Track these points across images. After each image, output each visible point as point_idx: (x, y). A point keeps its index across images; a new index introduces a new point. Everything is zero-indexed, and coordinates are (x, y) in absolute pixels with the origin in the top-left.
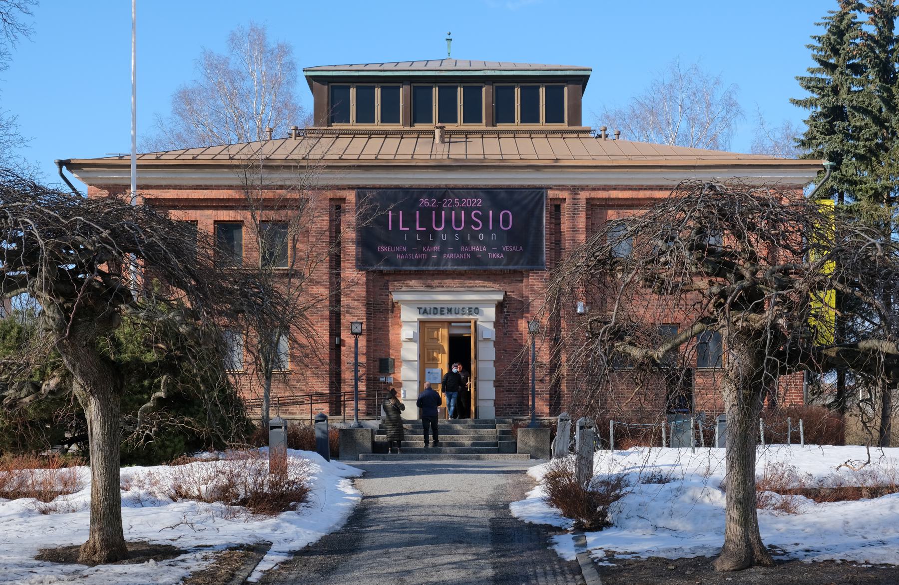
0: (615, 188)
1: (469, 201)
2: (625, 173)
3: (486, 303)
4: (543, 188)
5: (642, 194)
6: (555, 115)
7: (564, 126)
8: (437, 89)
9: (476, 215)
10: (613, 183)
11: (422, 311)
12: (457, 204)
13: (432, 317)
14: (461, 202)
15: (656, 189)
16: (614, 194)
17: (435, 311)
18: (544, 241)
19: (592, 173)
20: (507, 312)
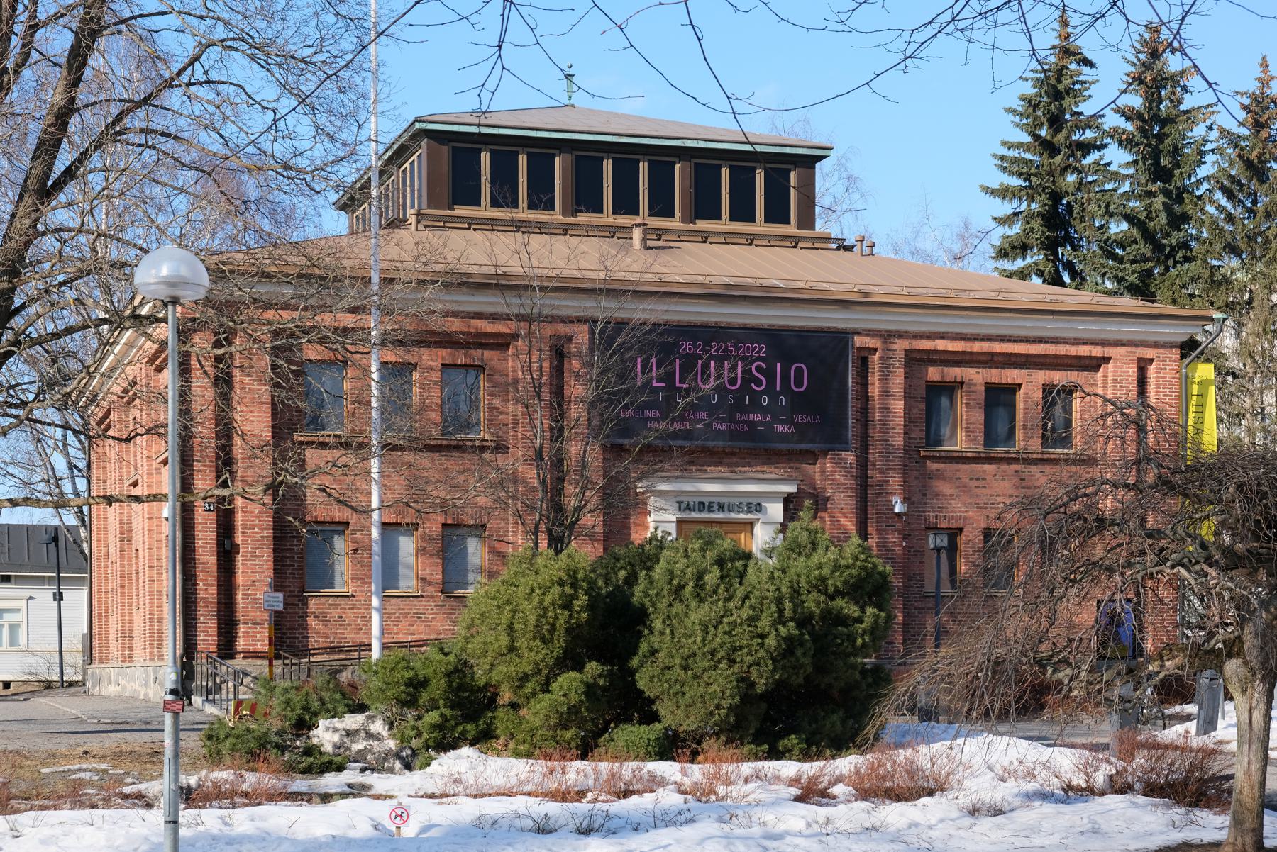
0: (943, 337)
1: (748, 347)
2: (962, 317)
3: (771, 496)
4: (848, 333)
5: (978, 347)
6: (777, 213)
7: (790, 230)
8: (610, 161)
9: (759, 369)
10: (942, 330)
11: (683, 506)
12: (731, 351)
13: (695, 515)
14: (738, 349)
15: (996, 340)
16: (941, 345)
17: (701, 506)
18: (850, 409)
19: (918, 314)
20: (795, 509)
